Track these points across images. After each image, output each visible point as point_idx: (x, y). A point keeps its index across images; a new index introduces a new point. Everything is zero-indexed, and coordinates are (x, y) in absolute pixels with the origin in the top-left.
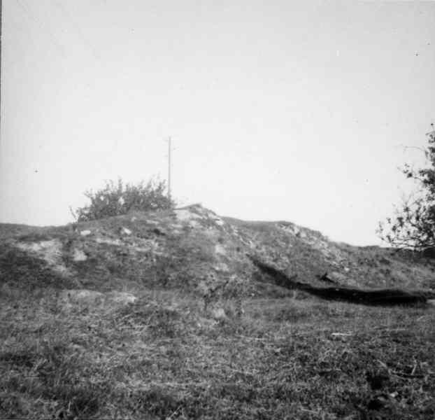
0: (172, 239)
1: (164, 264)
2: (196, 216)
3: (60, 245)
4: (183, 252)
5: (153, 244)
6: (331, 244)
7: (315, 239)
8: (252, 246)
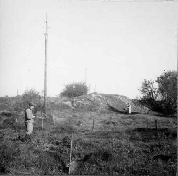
0: (92, 101)
1: (92, 107)
2: (96, 95)
3: (71, 102)
4: (94, 104)
5: (88, 103)
6: (128, 100)
7: (124, 99)
8: (108, 102)
